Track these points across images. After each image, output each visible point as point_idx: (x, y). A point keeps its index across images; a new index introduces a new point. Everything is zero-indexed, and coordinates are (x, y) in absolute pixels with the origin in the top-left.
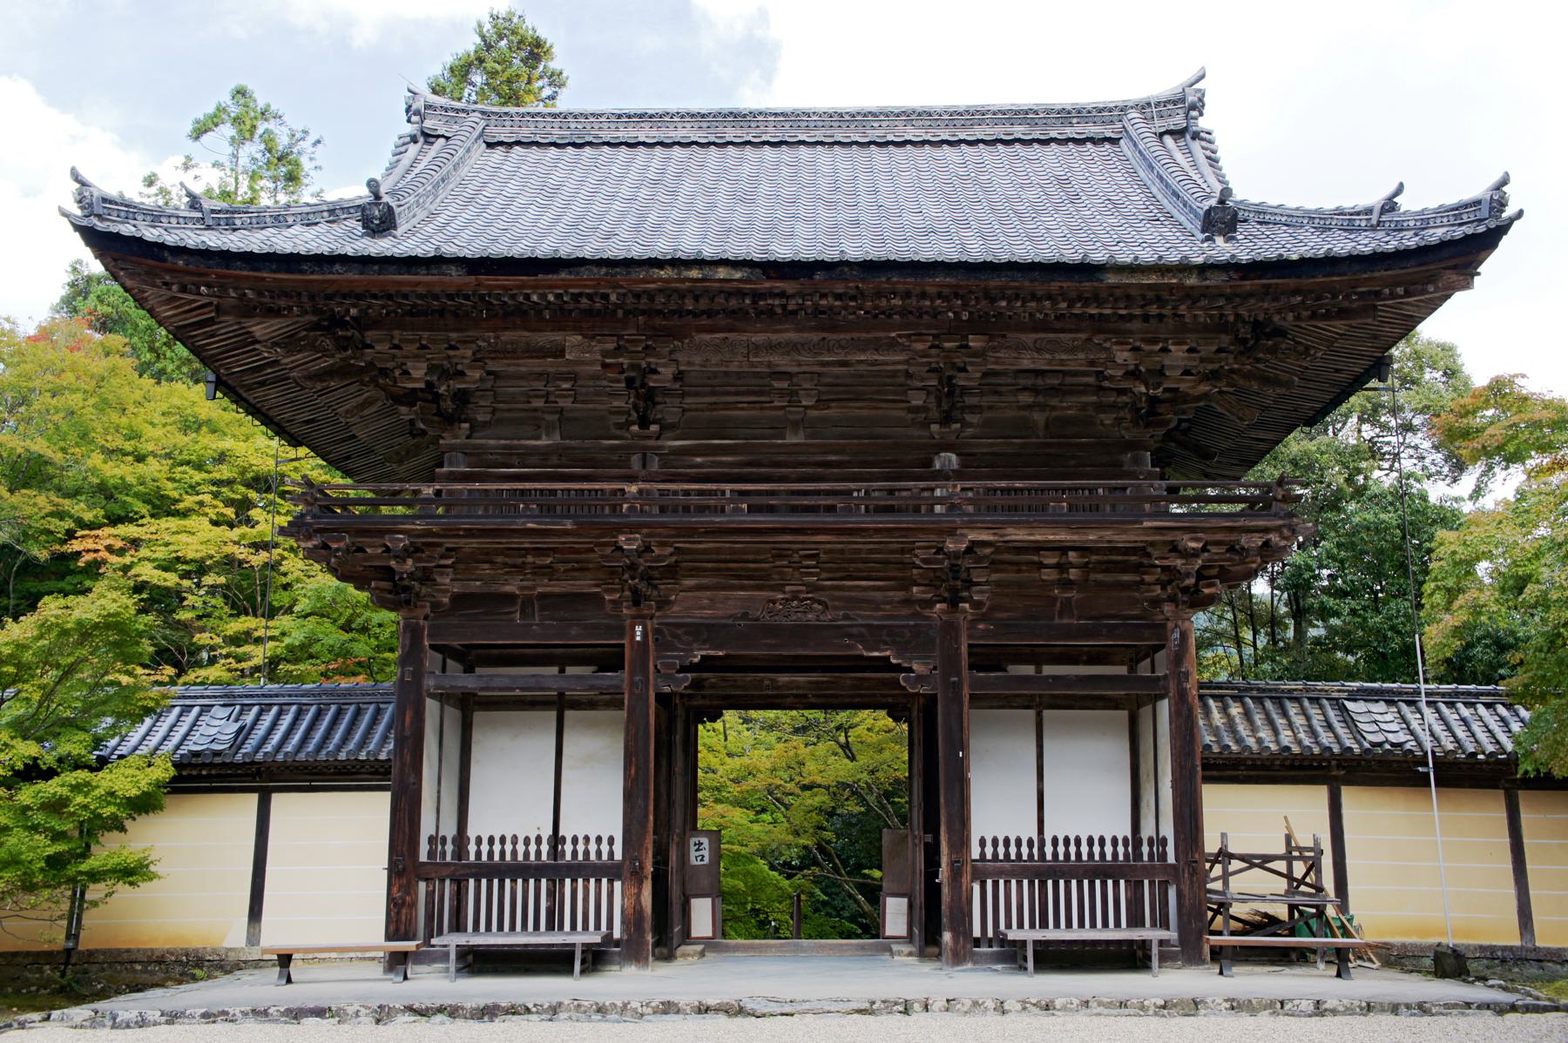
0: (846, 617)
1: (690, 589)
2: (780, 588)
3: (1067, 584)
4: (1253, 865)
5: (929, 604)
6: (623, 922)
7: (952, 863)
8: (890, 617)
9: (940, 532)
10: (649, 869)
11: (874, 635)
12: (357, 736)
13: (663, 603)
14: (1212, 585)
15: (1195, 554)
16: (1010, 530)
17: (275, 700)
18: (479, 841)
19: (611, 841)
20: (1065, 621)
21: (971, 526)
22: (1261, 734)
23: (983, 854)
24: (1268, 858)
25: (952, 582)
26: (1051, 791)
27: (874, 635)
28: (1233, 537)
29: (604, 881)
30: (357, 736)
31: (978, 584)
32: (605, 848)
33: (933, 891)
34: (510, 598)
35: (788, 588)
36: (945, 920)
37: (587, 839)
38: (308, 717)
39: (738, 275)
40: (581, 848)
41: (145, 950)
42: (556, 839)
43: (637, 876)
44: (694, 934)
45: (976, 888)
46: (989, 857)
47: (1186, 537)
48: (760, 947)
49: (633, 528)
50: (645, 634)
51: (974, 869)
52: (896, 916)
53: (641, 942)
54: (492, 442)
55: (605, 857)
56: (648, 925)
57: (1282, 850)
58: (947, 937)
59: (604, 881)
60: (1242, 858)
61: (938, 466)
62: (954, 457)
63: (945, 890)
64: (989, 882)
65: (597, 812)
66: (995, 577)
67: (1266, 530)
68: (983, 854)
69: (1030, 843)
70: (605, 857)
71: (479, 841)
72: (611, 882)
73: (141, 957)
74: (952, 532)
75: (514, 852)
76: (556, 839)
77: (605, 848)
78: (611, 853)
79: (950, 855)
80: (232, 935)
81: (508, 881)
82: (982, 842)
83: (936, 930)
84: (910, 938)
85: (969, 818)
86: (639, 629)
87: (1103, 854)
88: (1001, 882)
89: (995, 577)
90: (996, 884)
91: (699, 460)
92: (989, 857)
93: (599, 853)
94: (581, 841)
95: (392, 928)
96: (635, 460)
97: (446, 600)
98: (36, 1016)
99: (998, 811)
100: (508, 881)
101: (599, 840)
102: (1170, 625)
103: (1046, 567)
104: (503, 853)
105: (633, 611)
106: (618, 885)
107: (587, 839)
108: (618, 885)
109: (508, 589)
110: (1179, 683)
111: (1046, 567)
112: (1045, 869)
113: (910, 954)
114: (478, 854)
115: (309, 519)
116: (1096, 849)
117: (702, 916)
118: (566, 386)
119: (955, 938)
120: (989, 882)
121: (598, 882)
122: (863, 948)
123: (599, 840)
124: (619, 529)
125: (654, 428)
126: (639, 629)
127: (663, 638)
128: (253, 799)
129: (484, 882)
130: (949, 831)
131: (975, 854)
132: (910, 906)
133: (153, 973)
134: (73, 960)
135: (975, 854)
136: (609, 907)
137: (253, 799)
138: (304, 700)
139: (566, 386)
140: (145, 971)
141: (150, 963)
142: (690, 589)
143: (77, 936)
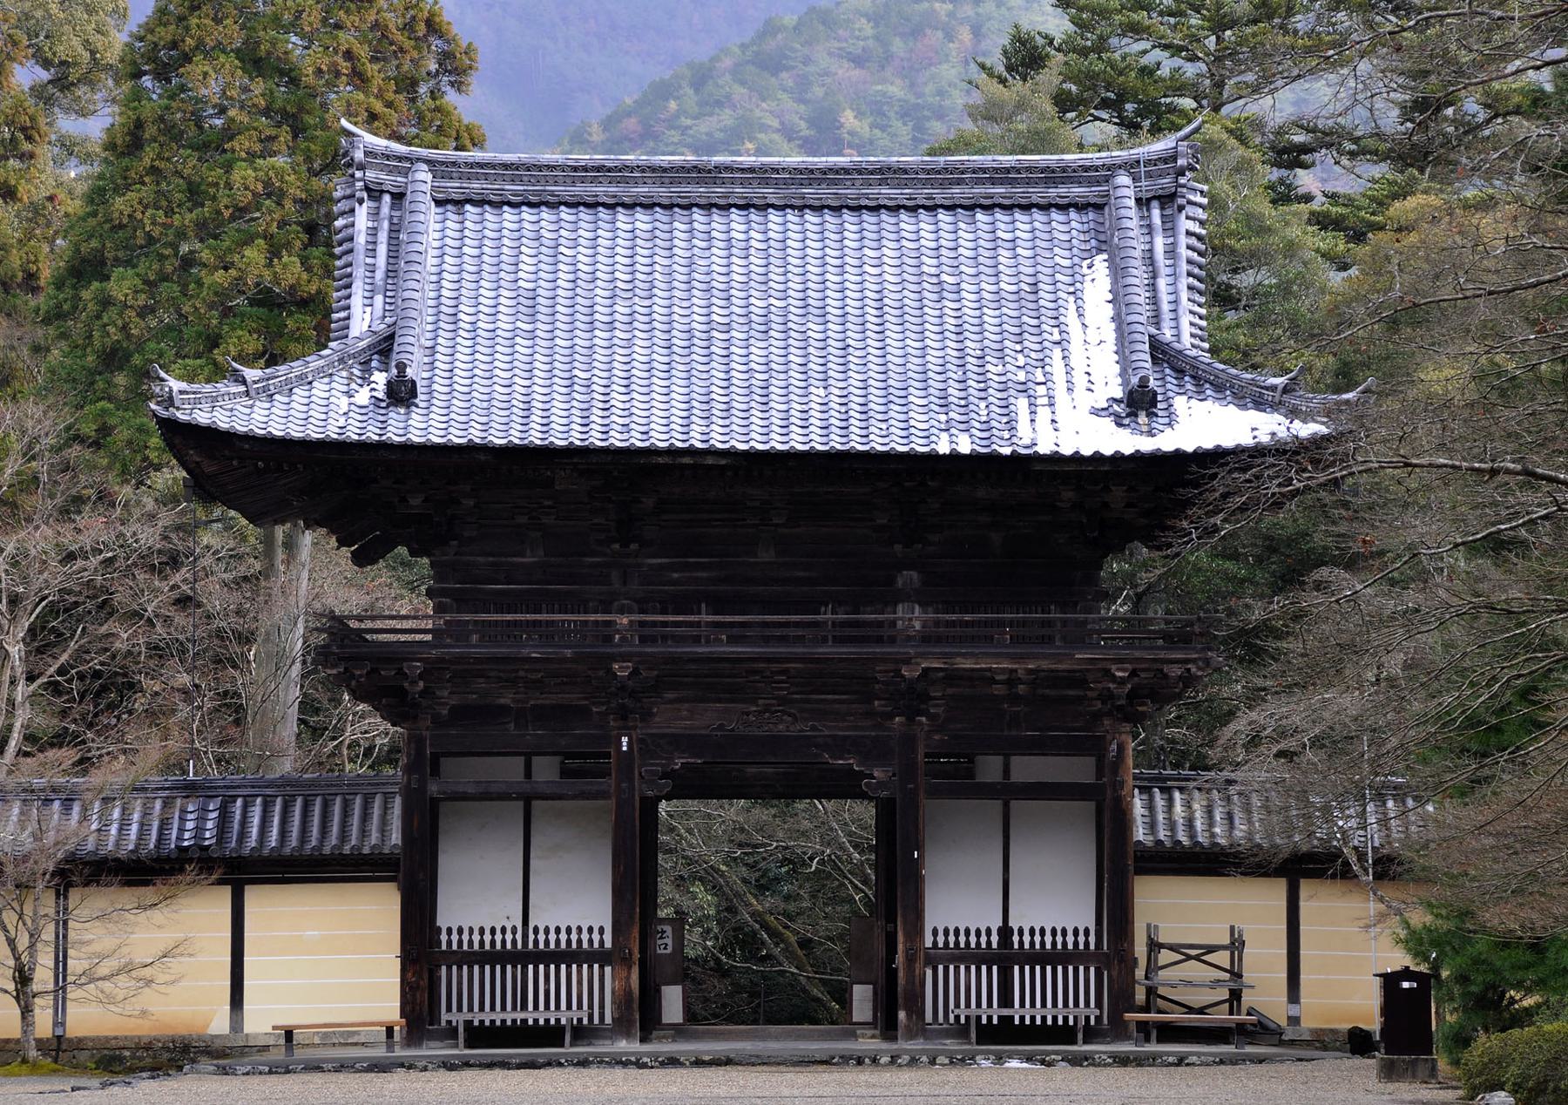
0: (813, 728)
1: (671, 702)
2: (754, 702)
3: (1015, 699)
4: (1189, 957)
5: (891, 716)
6: (613, 1002)
7: (906, 951)
8: (856, 728)
9: (897, 661)
10: (637, 955)
11: (840, 746)
12: (335, 830)
13: (647, 716)
14: (1144, 704)
15: (1122, 681)
16: (958, 660)
17: (221, 791)
18: (449, 931)
19: (601, 931)
20: (1014, 733)
21: (924, 656)
22: (1217, 830)
23: (935, 943)
24: (1211, 949)
25: (912, 698)
26: (1006, 889)
27: (840, 746)
28: (1159, 666)
29: (596, 966)
30: (335, 830)
31: (935, 698)
32: (596, 937)
33: (892, 974)
34: (504, 709)
35: (761, 702)
36: (900, 1001)
37: (580, 929)
38: (278, 808)
39: (723, 462)
40: (574, 937)
41: (132, 1038)
42: (1005, 932)
43: (626, 962)
44: (664, 1021)
45: (929, 972)
46: (941, 945)
47: (1114, 667)
48: (730, 1032)
49: (624, 657)
50: (630, 744)
51: (927, 955)
52: (862, 996)
53: (630, 1023)
54: (480, 559)
55: (596, 945)
56: (636, 1006)
57: (1227, 941)
58: (902, 1015)
59: (596, 966)
60: (1173, 948)
61: (900, 582)
62: (915, 575)
63: (901, 974)
64: (941, 968)
65: (578, 904)
66: (950, 691)
67: (1187, 661)
68: (935, 943)
69: (1087, 932)
70: (596, 945)
71: (449, 931)
72: (602, 968)
73: (128, 1044)
74: (907, 661)
75: (471, 942)
76: (1005, 932)
77: (596, 937)
78: (602, 942)
79: (905, 943)
80: (219, 1024)
81: (509, 967)
82: (935, 932)
83: (896, 1010)
84: (873, 1024)
85: (923, 910)
86: (625, 740)
87: (1043, 943)
88: (952, 967)
89: (950, 691)
90: (946, 970)
91: (676, 575)
92: (941, 945)
93: (591, 941)
94: (574, 931)
95: (408, 1008)
96: (615, 575)
97: (445, 712)
98: (95, 1082)
99: (957, 905)
100: (509, 967)
101: (558, 930)
102: (1109, 737)
103: (997, 682)
104: (504, 942)
105: (620, 723)
106: (608, 970)
107: (580, 929)
108: (608, 970)
109: (502, 701)
110: (1115, 790)
111: (997, 682)
112: (1006, 955)
113: (873, 1037)
114: (449, 943)
115: (335, 649)
116: (1037, 939)
117: (673, 1002)
118: (547, 503)
119: (909, 1016)
120: (941, 968)
121: (591, 967)
122: (828, 1032)
123: (590, 930)
124: (613, 658)
125: (634, 546)
126: (625, 740)
127: (644, 747)
128: (226, 892)
129: (487, 968)
130: (905, 923)
131: (929, 944)
132: (875, 993)
133: (141, 1059)
134: (64, 1047)
135: (929, 944)
136: (592, 993)
137: (226, 892)
138: (268, 791)
139: (547, 503)
140: (133, 1057)
141: (138, 1049)
142: (671, 702)
143: (63, 1024)
